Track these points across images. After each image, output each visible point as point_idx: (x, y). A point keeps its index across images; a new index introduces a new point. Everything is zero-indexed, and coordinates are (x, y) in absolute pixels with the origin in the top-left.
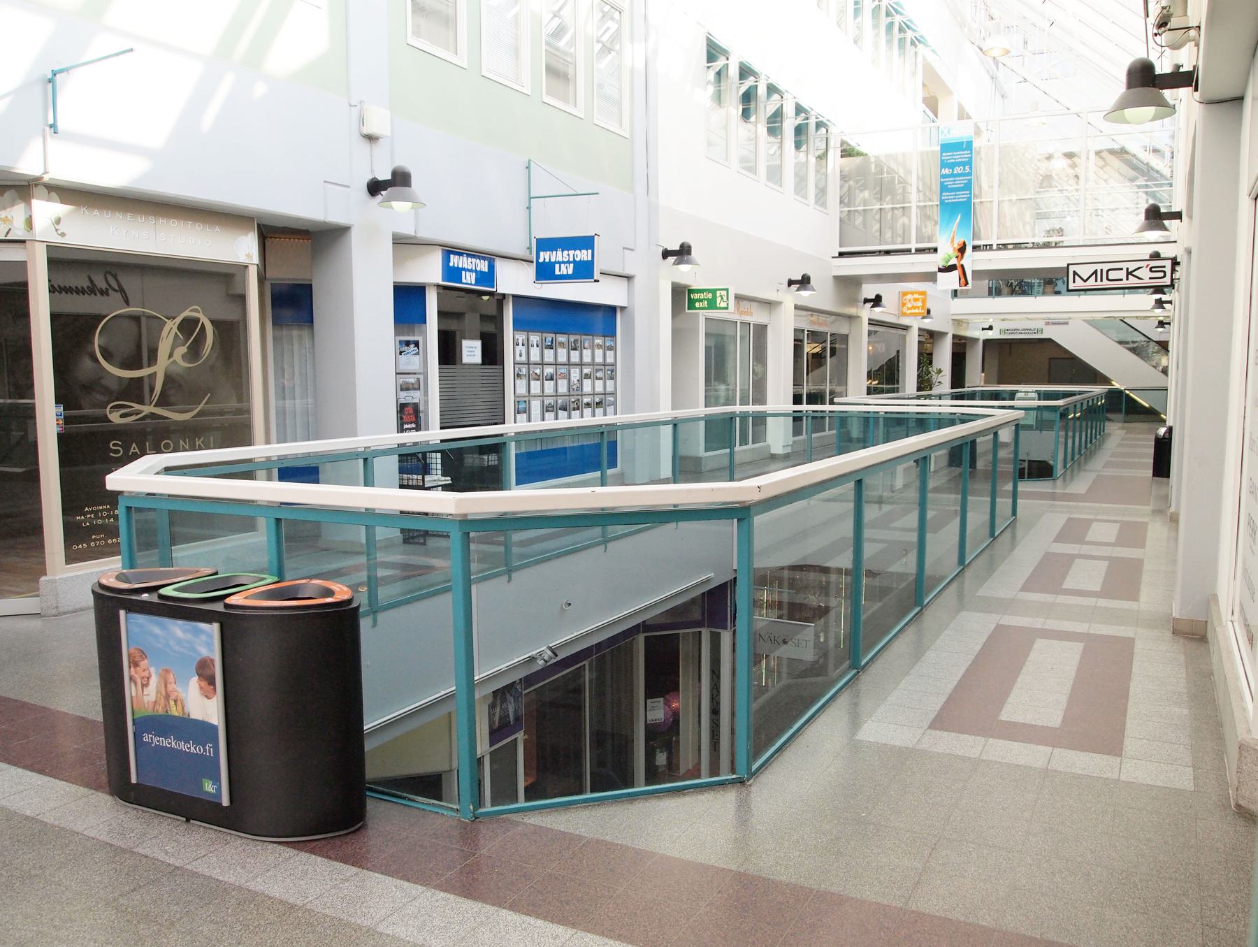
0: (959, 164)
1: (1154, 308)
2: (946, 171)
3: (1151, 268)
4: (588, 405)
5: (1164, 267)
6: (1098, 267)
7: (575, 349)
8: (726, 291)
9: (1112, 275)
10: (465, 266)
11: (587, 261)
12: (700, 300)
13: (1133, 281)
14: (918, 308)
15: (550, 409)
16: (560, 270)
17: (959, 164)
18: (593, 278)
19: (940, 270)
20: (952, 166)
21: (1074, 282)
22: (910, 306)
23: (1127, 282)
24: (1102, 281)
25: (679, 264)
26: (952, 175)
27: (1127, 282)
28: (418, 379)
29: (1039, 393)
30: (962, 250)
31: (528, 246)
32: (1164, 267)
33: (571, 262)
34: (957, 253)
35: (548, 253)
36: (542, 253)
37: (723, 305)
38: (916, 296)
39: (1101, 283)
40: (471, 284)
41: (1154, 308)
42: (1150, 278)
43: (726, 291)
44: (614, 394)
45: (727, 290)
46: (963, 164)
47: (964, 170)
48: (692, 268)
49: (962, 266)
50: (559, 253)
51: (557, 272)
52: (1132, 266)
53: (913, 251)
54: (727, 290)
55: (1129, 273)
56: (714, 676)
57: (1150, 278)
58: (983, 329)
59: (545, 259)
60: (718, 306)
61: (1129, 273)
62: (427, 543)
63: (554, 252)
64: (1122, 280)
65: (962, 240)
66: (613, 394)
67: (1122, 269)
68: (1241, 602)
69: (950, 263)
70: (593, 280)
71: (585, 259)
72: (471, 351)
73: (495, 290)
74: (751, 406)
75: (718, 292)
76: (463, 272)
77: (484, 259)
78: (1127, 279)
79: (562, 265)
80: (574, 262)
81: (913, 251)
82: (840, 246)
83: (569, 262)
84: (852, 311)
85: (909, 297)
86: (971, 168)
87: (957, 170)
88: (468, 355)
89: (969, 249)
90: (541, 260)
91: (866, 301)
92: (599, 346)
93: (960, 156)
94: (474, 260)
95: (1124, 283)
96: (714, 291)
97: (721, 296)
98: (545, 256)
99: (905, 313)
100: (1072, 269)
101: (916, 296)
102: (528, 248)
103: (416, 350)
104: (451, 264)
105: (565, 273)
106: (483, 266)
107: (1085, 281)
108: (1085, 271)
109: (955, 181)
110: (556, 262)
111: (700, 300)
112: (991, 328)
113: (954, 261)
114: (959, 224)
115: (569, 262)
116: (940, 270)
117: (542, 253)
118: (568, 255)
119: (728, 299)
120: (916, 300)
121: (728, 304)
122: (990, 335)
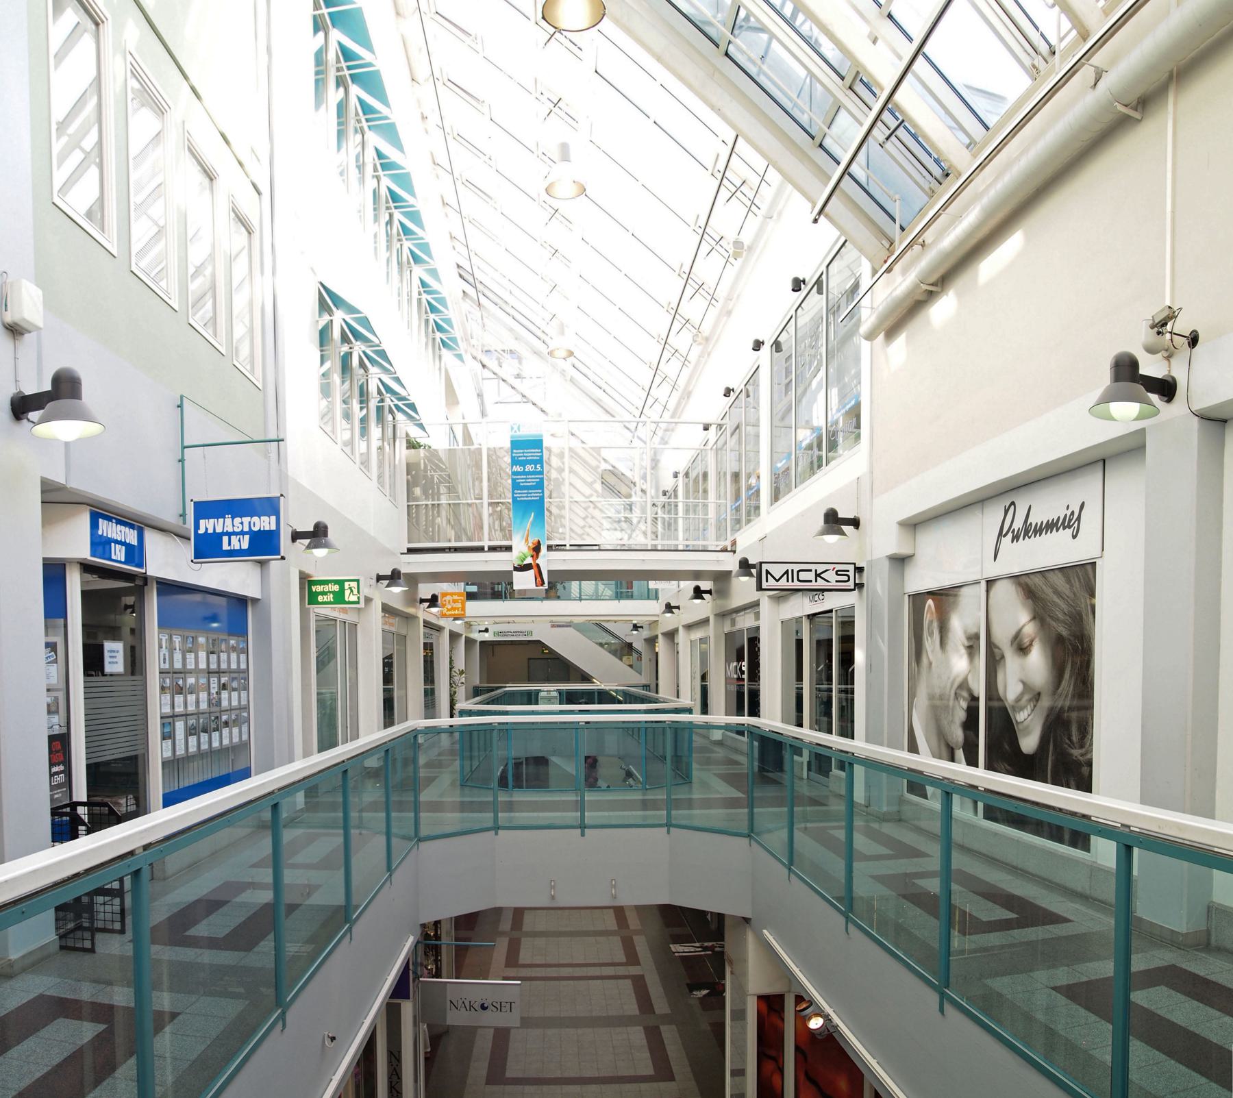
0: (530, 462)
1: (664, 612)
2: (518, 468)
3: (837, 571)
4: (226, 724)
5: (848, 571)
6: (789, 567)
7: (212, 653)
8: (356, 583)
9: (803, 576)
10: (115, 536)
11: (270, 531)
12: (323, 593)
13: (821, 583)
14: (458, 609)
15: (193, 732)
16: (230, 544)
17: (530, 462)
18: (279, 554)
19: (516, 569)
20: (523, 463)
21: (767, 581)
22: (449, 607)
23: (816, 584)
24: (793, 581)
25: (316, 547)
26: (524, 473)
27: (816, 584)
28: (56, 698)
29: (560, 692)
30: (537, 549)
31: (181, 512)
32: (848, 571)
33: (246, 533)
34: (532, 553)
35: (212, 521)
36: (202, 522)
37: (354, 598)
38: (455, 597)
39: (792, 584)
40: (120, 562)
41: (664, 612)
42: (837, 581)
43: (356, 583)
44: (247, 708)
45: (358, 581)
46: (535, 462)
47: (535, 468)
48: (839, 539)
49: (538, 565)
50: (228, 520)
51: (225, 547)
52: (820, 568)
53: (486, 549)
54: (358, 581)
55: (818, 575)
56: (397, 1056)
57: (837, 581)
58: (480, 631)
59: (207, 529)
60: (347, 599)
61: (818, 575)
62: (97, 949)
63: (221, 520)
64: (811, 581)
65: (536, 539)
66: (246, 708)
67: (811, 571)
68: (974, 892)
69: (525, 562)
70: (279, 557)
71: (267, 528)
72: (115, 655)
73: (144, 571)
74: (746, 718)
75: (346, 584)
76: (113, 544)
77: (132, 526)
78: (816, 581)
79: (233, 537)
80: (250, 532)
81: (486, 549)
82: (409, 542)
83: (243, 533)
84: (411, 610)
85: (448, 598)
86: (542, 467)
87: (529, 468)
88: (110, 663)
89: (544, 549)
90: (201, 531)
91: (422, 601)
92: (234, 649)
93: (531, 454)
94: (123, 528)
95: (813, 585)
96: (341, 583)
97: (350, 588)
98: (207, 525)
99: (445, 615)
100: (764, 567)
101: (455, 597)
102: (181, 516)
103: (52, 656)
104: (100, 533)
105: (237, 547)
106: (131, 537)
107: (777, 581)
108: (777, 571)
109: (526, 479)
110: (223, 534)
111: (323, 593)
112: (487, 630)
113: (529, 560)
114: (532, 524)
115: (243, 533)
116: (516, 569)
117: (202, 522)
118: (242, 523)
119: (358, 592)
120: (455, 601)
121: (358, 598)
122: (487, 637)
